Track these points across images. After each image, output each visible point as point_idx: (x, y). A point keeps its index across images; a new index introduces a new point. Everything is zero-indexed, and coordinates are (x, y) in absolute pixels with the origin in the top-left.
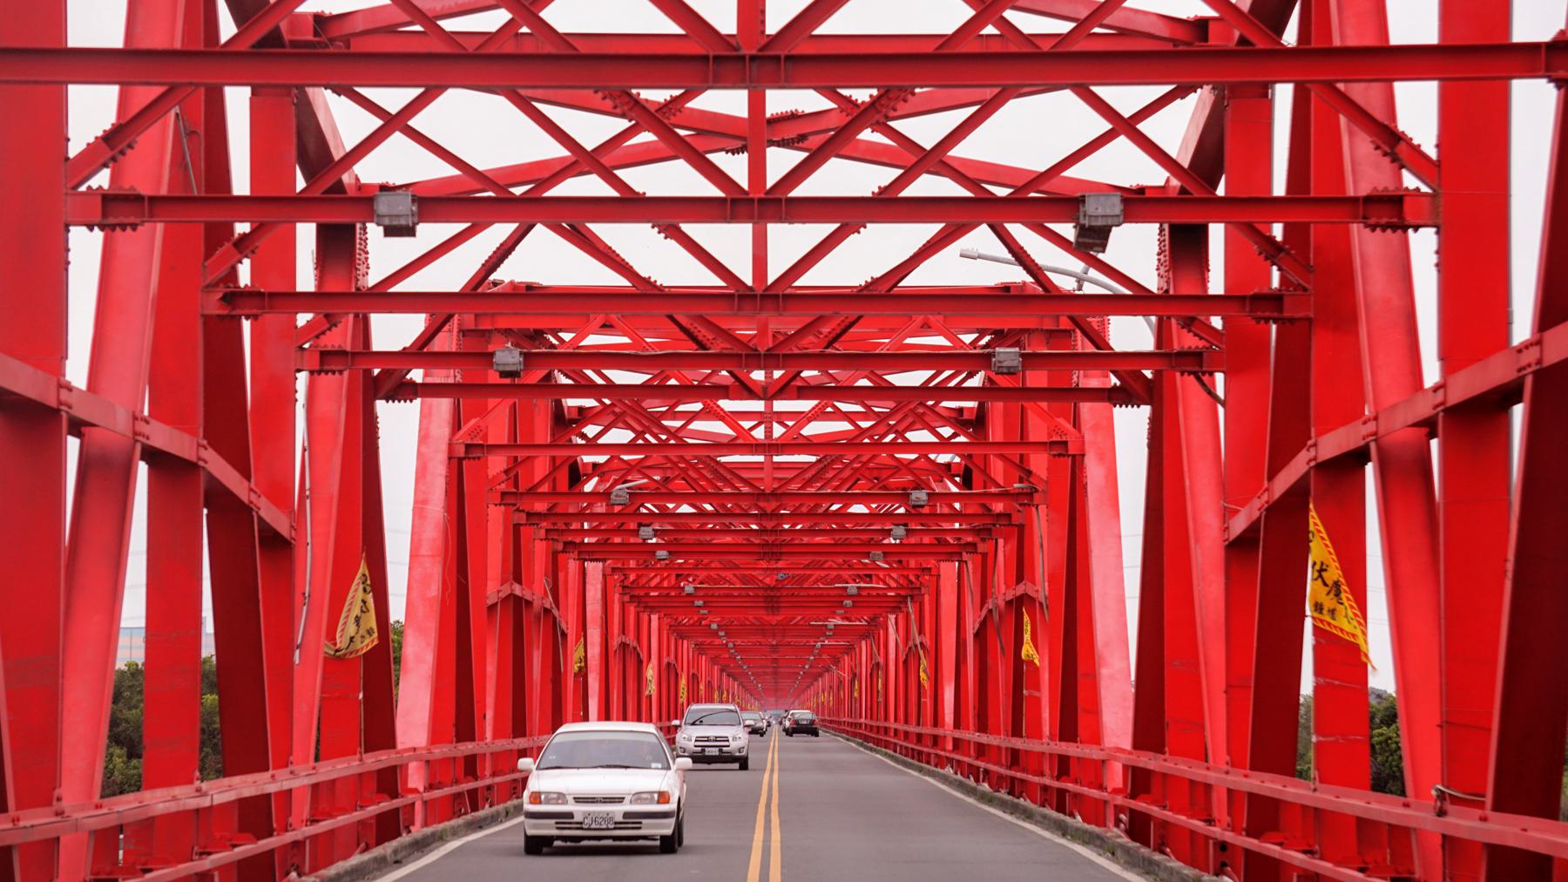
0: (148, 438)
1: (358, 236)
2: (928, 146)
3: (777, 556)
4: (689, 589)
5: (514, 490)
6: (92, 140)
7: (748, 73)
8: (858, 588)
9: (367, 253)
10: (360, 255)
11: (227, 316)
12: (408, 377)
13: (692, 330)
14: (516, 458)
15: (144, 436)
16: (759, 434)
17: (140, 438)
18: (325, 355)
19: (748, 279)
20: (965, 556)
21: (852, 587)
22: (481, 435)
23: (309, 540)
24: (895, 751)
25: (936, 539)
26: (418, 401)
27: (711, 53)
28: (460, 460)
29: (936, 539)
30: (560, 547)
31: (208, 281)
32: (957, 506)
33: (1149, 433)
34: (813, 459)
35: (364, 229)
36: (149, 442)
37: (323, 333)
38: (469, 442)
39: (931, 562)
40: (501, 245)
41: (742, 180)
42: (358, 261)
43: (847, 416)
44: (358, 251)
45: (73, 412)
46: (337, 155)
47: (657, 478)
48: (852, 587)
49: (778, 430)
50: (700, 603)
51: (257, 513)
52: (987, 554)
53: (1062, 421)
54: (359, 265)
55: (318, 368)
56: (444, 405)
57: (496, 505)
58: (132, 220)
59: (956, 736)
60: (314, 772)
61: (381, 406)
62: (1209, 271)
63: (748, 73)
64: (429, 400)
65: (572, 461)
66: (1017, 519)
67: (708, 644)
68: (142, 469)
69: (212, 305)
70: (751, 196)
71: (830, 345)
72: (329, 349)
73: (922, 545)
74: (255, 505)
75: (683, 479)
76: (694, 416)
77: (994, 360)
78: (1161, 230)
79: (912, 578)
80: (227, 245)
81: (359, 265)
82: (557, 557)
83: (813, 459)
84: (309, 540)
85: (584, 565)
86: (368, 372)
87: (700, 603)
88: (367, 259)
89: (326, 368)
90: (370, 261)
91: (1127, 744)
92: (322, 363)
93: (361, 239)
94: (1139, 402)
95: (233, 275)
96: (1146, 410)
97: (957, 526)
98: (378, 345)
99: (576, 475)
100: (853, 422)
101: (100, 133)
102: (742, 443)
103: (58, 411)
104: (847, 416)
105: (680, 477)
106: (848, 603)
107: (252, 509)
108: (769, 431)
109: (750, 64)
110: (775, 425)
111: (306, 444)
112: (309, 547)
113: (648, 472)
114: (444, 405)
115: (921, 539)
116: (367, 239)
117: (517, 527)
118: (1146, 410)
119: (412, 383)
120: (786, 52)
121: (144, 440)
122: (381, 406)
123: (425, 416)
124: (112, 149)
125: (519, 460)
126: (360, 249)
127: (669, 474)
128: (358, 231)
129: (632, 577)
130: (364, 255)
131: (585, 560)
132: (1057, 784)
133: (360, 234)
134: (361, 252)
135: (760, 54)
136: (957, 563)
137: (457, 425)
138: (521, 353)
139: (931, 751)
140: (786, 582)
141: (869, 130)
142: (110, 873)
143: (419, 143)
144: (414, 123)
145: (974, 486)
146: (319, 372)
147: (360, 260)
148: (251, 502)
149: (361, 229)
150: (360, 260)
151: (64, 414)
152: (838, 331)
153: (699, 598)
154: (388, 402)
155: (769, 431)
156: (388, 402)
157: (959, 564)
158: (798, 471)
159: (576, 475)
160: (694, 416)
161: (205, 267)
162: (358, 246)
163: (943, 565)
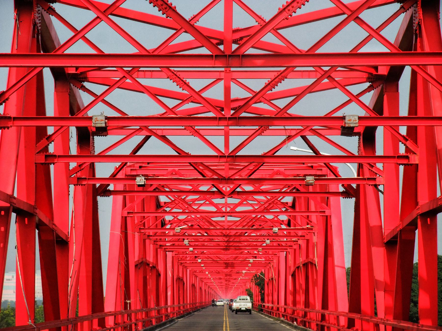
0: (15, 204)
1: (91, 141)
2: (282, 107)
3: (229, 249)
4: (199, 261)
5: (143, 228)
8: (253, 260)
9: (94, 147)
10: (92, 147)
12: (108, 189)
13: (202, 173)
15: (14, 203)
17: (12, 204)
18: (79, 179)
19: (223, 150)
20: (289, 250)
21: (251, 260)
22: (133, 209)
24: (271, 315)
25: (278, 244)
26: (111, 197)
28: (126, 217)
30: (158, 246)
32: (285, 232)
33: (355, 207)
34: (238, 219)
35: (93, 139)
36: (16, 206)
38: (128, 211)
41: (233, 86)
43: (251, 205)
49: (228, 209)
50: (203, 265)
51: (55, 232)
52: (296, 249)
53: (323, 204)
54: (91, 151)
55: (76, 183)
56: (120, 198)
61: (99, 198)
62: (376, 152)
64: (115, 196)
66: (307, 237)
67: (229, 279)
69: (41, 159)
71: (250, 176)
74: (54, 229)
75: (198, 225)
76: (201, 205)
77: (306, 180)
78: (359, 139)
79: (270, 257)
81: (91, 151)
82: (157, 250)
83: (238, 219)
86: (94, 185)
87: (203, 265)
90: (95, 150)
91: (347, 310)
92: (78, 182)
93: (92, 142)
94: (351, 197)
95: (46, 149)
96: (354, 199)
97: (285, 240)
99: (163, 224)
100: (253, 207)
102: (219, 212)
104: (251, 205)
106: (250, 265)
107: (53, 231)
110: (228, 208)
111: (74, 210)
112: (74, 244)
114: (120, 198)
115: (273, 244)
116: (94, 142)
117: (144, 241)
118: (354, 199)
121: (14, 205)
122: (99, 198)
123: (114, 202)
127: (193, 224)
128: (91, 139)
129: (289, 199)
130: (93, 147)
131: (167, 251)
132: (321, 323)
134: (92, 146)
135: (232, 54)
137: (124, 205)
138: (145, 179)
139: (271, 311)
141: (215, 176)
144: (107, 99)
145: (291, 226)
146: (77, 185)
147: (92, 149)
148: (53, 228)
149: (92, 139)
152: (251, 173)
153: (202, 263)
154: (101, 197)
156: (101, 197)
159: (163, 224)
160: (201, 205)
161: (36, 146)
162: (91, 144)
163: (281, 253)
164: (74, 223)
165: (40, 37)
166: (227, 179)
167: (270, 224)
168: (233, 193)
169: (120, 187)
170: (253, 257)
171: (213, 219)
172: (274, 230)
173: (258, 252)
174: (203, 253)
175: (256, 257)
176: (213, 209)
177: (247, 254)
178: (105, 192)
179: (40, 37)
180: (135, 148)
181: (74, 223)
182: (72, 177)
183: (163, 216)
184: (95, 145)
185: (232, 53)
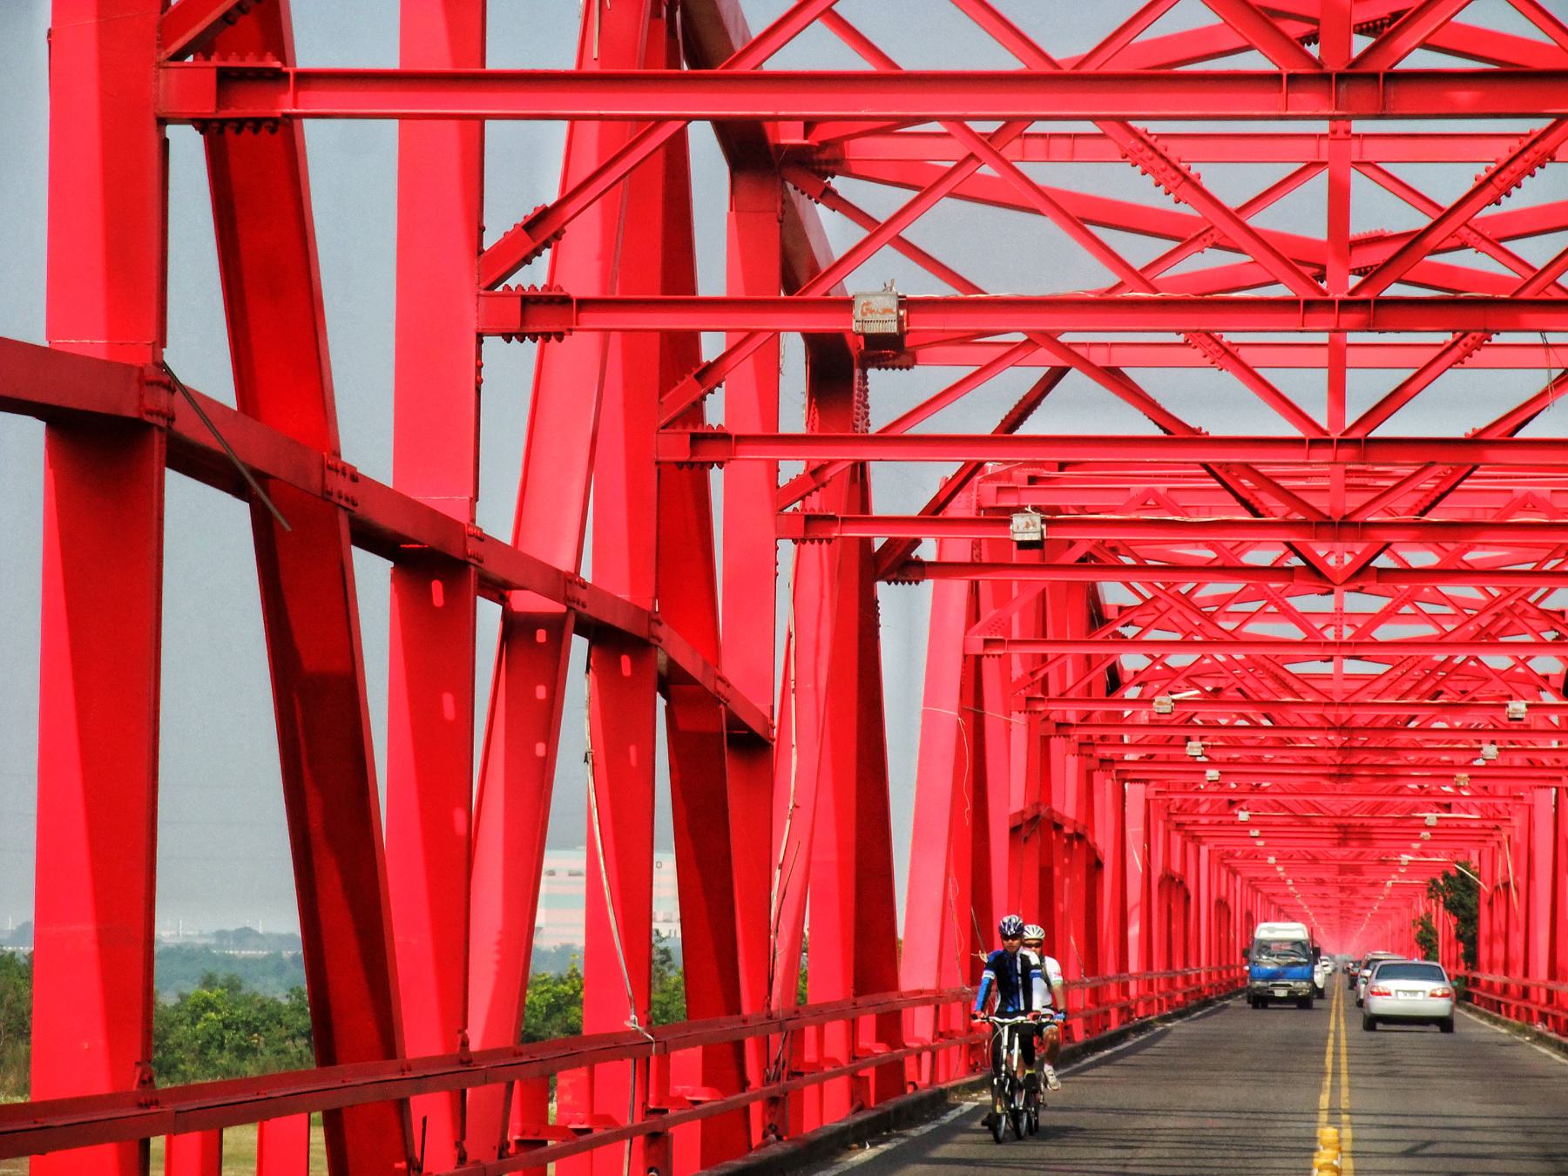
4: (1243, 816)
6: (510, 228)
7: (1151, 1122)
8: (1438, 818)
9: (868, 407)
11: (687, 463)
12: (914, 555)
14: (1044, 657)
16: (1330, 634)
17: (575, 606)
19: (1322, 419)
21: (1431, 818)
23: (794, 742)
25: (1529, 760)
27: (1285, 71)
29: (1529, 760)
30: (1093, 763)
31: (662, 422)
32: (1555, 719)
35: (865, 378)
37: (809, 494)
39: (1522, 789)
40: (1025, 398)
42: (855, 416)
43: (1431, 618)
44: (856, 404)
45: (358, 511)
46: (824, 266)
47: (1209, 689)
48: (1431, 818)
49: (1348, 633)
56: (958, 588)
57: (1020, 712)
58: (557, 328)
59: (1551, 988)
60: (797, 1016)
61: (882, 588)
63: (1151, 1122)
65: (1110, 662)
68: (579, 646)
69: (675, 448)
70: (1330, 296)
71: (1423, 513)
72: (817, 513)
73: (1511, 767)
75: (1239, 690)
76: (1251, 616)
80: (689, 378)
84: (794, 742)
85: (1123, 786)
86: (867, 543)
87: (1255, 833)
88: (867, 414)
89: (811, 535)
93: (860, 390)
95: (697, 410)
97: (1555, 745)
98: (879, 508)
100: (1439, 626)
101: (520, 220)
103: (466, 564)
104: (1431, 618)
105: (1234, 688)
106: (1426, 834)
108: (1339, 634)
109: (1336, 83)
112: (794, 750)
113: (1199, 681)
114: (958, 588)
119: (919, 563)
120: (1385, 68)
121: (580, 609)
122: (882, 588)
124: (534, 241)
125: (1049, 660)
126: (858, 402)
127: (1222, 684)
128: (856, 380)
130: (863, 410)
133: (859, 384)
134: (860, 405)
136: (1554, 790)
138: (1043, 521)
139: (1501, 999)
140: (1354, 810)
142: (538, 1134)
143: (925, 266)
144: (910, 234)
146: (804, 541)
148: (719, 693)
149: (859, 378)
150: (858, 414)
151: (473, 569)
155: (1339, 634)
157: (1557, 792)
158: (1366, 682)
159: (1115, 680)
160: (1251, 616)
161: (661, 403)
163: (1540, 793)
164: (793, 677)
165: (678, 14)
166: (1340, 523)
167: (1499, 687)
168: (1362, 576)
169: (960, 550)
170: (1437, 804)
171: (1294, 668)
172: (1510, 709)
173: (1457, 787)
174: (1256, 789)
175: (1448, 808)
176: (1293, 632)
177: (1415, 794)
178: (903, 566)
179: (678, 14)
180: (1011, 413)
181: (793, 677)
182: (499, 295)
183: (1109, 656)
184: (870, 401)
185: (1349, 67)
